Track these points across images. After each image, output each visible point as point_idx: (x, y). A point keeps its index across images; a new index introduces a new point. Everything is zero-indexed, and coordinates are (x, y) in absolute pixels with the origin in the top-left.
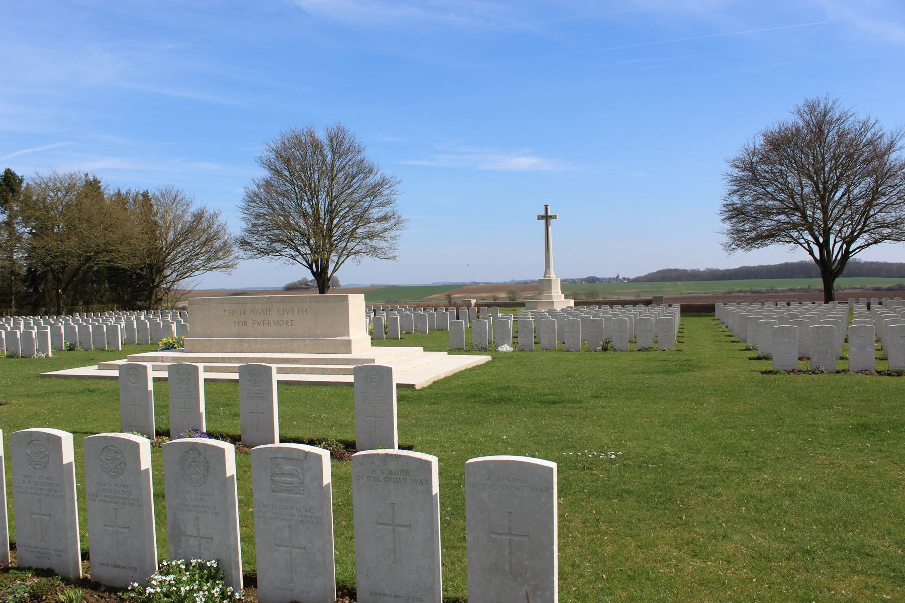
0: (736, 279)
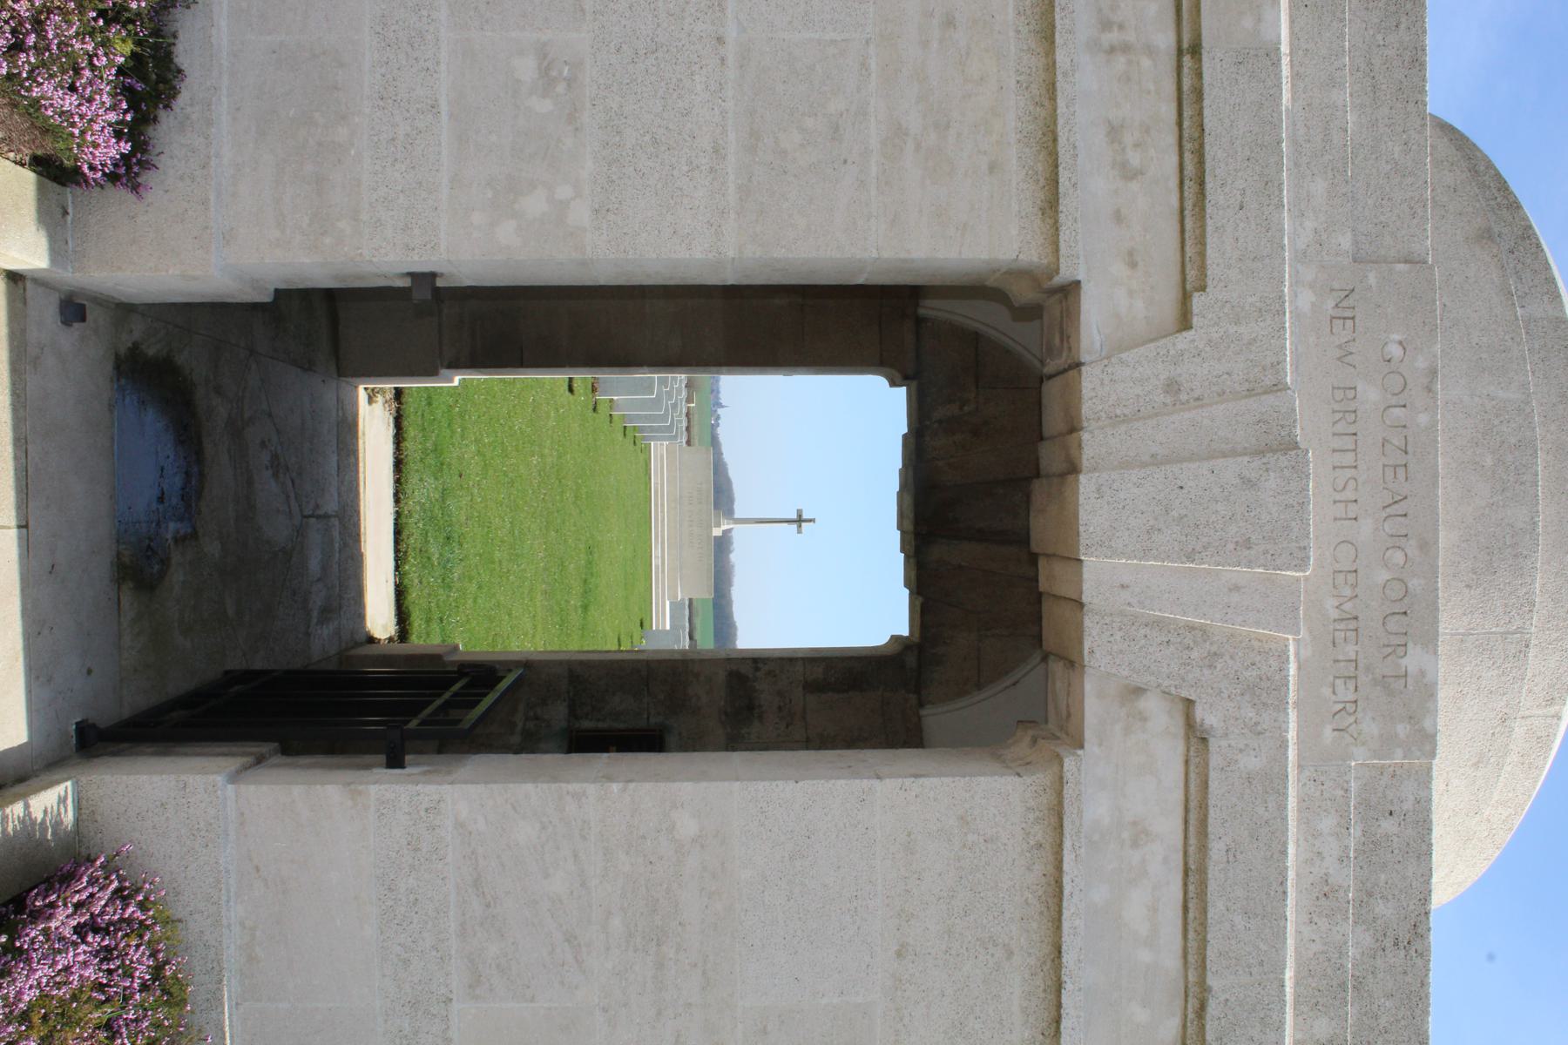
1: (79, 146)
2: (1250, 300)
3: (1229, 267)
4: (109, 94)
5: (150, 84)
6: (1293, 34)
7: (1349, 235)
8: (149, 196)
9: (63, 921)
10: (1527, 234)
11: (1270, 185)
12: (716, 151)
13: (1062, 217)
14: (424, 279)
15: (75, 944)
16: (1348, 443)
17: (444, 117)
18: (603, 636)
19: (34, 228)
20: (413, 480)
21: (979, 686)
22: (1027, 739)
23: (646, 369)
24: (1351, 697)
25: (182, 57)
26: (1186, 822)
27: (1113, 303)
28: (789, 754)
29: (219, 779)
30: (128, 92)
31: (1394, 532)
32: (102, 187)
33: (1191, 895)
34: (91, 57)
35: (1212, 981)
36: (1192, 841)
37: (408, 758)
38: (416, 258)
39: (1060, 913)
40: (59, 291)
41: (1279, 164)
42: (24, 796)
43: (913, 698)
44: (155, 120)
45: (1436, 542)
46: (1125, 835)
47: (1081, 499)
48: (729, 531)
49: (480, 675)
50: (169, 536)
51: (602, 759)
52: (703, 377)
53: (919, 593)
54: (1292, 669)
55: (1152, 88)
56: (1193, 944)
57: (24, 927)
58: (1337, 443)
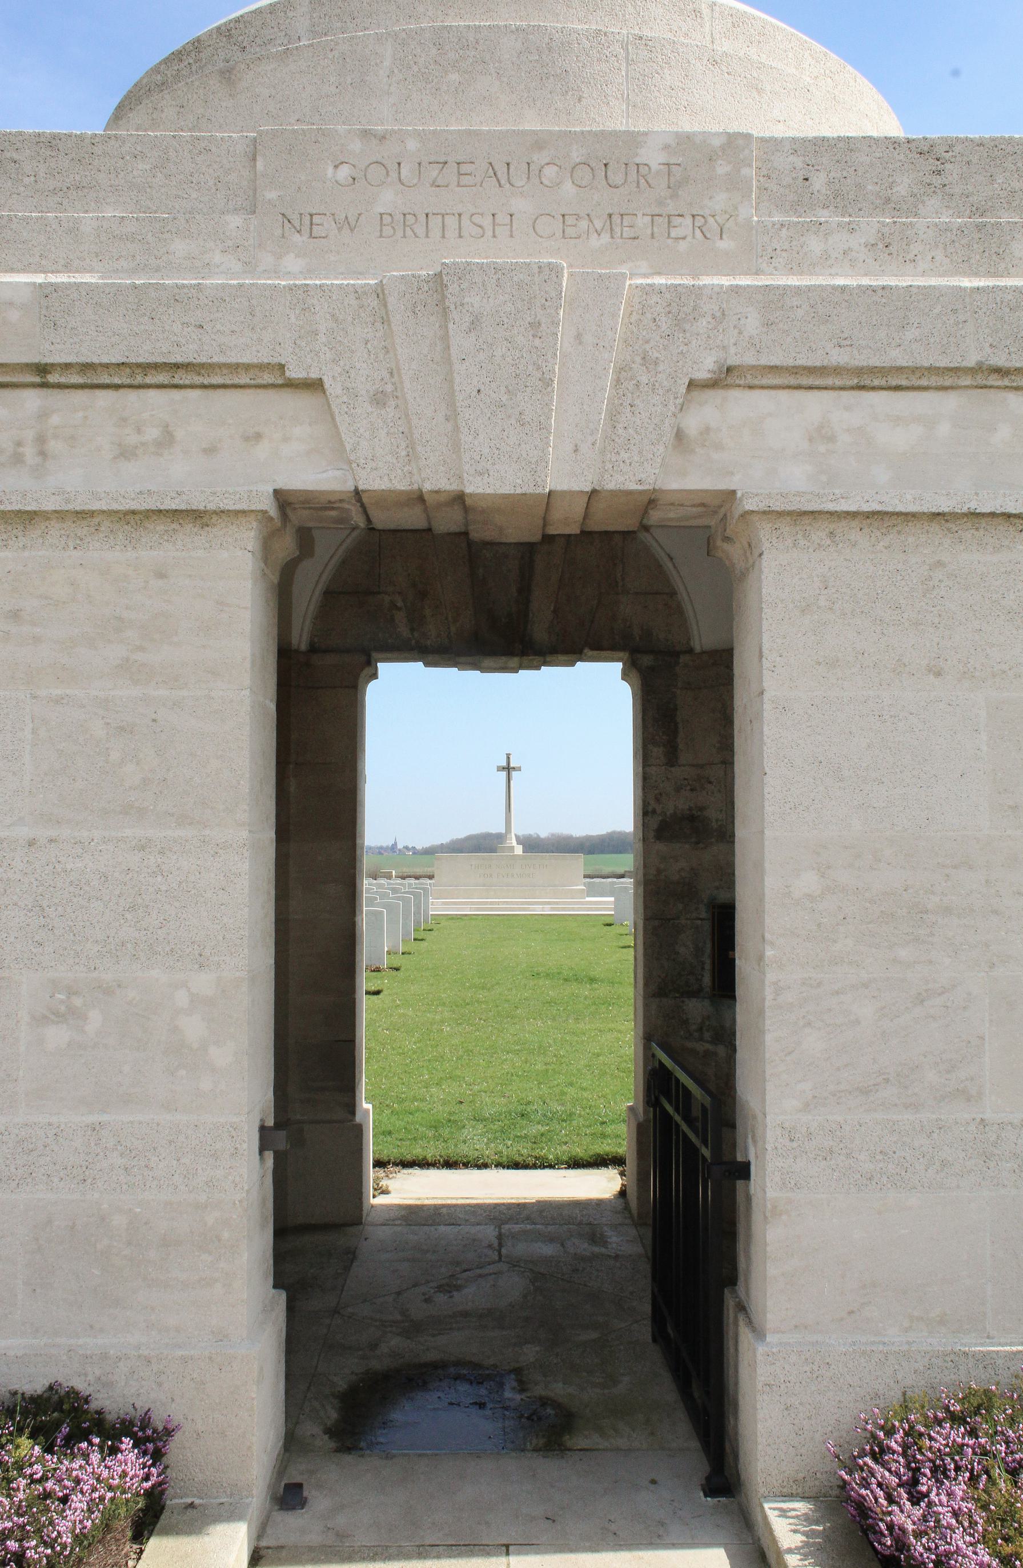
0: (602, 852)
1: (124, 1492)
2: (293, 320)
3: (260, 340)
4: (72, 1461)
5: (62, 1418)
6: (24, 270)
7: (228, 218)
8: (177, 1418)
9: (906, 1516)
10: (225, 32)
11: (178, 297)
12: (143, 848)
13: (211, 507)
14: (266, 1137)
15: (930, 1504)
16: (435, 222)
17: (105, 1118)
18: (620, 962)
19: (206, 1539)
20: (465, 1150)
21: (673, 594)
22: (726, 546)
23: (358, 919)
24: (689, 220)
25: (35, 1385)
26: (810, 388)
27: (299, 457)
28: (274, 749)
29: (761, 1349)
30: (70, 1441)
31: (524, 177)
32: (166, 1467)
33: (883, 383)
34: (33, 1481)
35: (971, 362)
36: (829, 381)
37: (740, 1158)
38: (245, 1146)
39: (898, 514)
40: (270, 1512)
41: (157, 287)
42: (779, 1554)
43: (684, 659)
44: (99, 1412)
45: (535, 133)
46: (822, 449)
47: (489, 491)
48: (517, 837)
49: (658, 1084)
50: (518, 1397)
51: (743, 965)
52: (366, 862)
53: (581, 652)
54: (660, 280)
55: (80, 414)
56: (934, 381)
57: (914, 1558)
58: (436, 232)
